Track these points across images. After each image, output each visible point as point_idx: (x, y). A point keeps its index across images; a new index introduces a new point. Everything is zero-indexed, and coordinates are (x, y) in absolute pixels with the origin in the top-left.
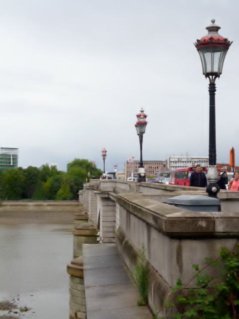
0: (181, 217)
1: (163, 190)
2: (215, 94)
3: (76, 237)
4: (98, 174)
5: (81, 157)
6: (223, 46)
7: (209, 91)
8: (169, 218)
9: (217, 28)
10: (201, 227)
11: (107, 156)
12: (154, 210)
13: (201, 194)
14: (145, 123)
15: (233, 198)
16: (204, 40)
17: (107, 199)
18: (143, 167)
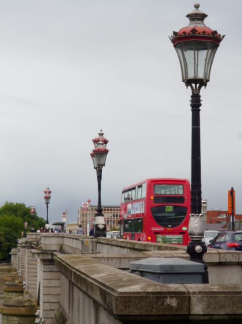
0: (139, 293)
1: (130, 249)
2: (199, 110)
3: (5, 317)
4: (39, 224)
5: (16, 200)
6: (211, 41)
7: (191, 105)
8: (121, 293)
9: (202, 17)
10: (170, 307)
11: (51, 199)
12: (103, 282)
13: (180, 255)
14: (106, 152)
15: (228, 261)
16: (184, 33)
17: (50, 261)
18: (102, 215)
